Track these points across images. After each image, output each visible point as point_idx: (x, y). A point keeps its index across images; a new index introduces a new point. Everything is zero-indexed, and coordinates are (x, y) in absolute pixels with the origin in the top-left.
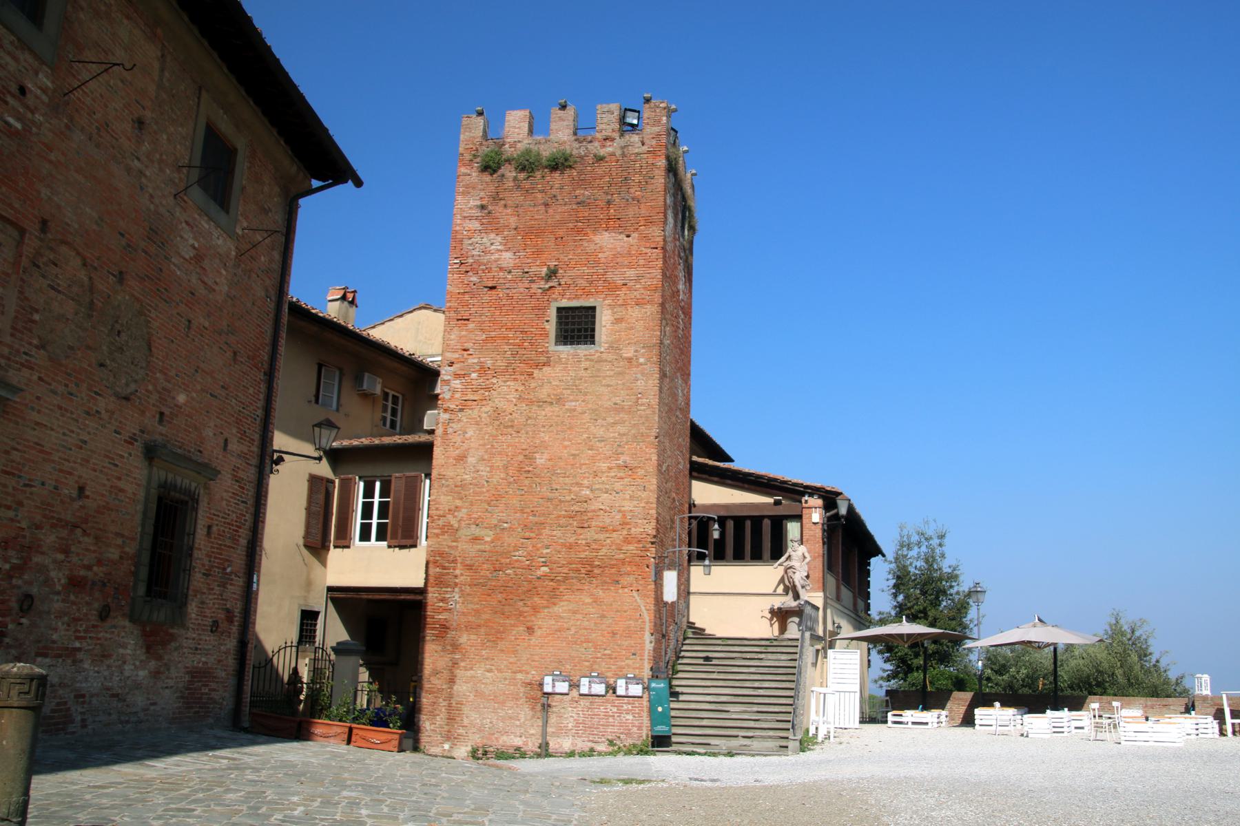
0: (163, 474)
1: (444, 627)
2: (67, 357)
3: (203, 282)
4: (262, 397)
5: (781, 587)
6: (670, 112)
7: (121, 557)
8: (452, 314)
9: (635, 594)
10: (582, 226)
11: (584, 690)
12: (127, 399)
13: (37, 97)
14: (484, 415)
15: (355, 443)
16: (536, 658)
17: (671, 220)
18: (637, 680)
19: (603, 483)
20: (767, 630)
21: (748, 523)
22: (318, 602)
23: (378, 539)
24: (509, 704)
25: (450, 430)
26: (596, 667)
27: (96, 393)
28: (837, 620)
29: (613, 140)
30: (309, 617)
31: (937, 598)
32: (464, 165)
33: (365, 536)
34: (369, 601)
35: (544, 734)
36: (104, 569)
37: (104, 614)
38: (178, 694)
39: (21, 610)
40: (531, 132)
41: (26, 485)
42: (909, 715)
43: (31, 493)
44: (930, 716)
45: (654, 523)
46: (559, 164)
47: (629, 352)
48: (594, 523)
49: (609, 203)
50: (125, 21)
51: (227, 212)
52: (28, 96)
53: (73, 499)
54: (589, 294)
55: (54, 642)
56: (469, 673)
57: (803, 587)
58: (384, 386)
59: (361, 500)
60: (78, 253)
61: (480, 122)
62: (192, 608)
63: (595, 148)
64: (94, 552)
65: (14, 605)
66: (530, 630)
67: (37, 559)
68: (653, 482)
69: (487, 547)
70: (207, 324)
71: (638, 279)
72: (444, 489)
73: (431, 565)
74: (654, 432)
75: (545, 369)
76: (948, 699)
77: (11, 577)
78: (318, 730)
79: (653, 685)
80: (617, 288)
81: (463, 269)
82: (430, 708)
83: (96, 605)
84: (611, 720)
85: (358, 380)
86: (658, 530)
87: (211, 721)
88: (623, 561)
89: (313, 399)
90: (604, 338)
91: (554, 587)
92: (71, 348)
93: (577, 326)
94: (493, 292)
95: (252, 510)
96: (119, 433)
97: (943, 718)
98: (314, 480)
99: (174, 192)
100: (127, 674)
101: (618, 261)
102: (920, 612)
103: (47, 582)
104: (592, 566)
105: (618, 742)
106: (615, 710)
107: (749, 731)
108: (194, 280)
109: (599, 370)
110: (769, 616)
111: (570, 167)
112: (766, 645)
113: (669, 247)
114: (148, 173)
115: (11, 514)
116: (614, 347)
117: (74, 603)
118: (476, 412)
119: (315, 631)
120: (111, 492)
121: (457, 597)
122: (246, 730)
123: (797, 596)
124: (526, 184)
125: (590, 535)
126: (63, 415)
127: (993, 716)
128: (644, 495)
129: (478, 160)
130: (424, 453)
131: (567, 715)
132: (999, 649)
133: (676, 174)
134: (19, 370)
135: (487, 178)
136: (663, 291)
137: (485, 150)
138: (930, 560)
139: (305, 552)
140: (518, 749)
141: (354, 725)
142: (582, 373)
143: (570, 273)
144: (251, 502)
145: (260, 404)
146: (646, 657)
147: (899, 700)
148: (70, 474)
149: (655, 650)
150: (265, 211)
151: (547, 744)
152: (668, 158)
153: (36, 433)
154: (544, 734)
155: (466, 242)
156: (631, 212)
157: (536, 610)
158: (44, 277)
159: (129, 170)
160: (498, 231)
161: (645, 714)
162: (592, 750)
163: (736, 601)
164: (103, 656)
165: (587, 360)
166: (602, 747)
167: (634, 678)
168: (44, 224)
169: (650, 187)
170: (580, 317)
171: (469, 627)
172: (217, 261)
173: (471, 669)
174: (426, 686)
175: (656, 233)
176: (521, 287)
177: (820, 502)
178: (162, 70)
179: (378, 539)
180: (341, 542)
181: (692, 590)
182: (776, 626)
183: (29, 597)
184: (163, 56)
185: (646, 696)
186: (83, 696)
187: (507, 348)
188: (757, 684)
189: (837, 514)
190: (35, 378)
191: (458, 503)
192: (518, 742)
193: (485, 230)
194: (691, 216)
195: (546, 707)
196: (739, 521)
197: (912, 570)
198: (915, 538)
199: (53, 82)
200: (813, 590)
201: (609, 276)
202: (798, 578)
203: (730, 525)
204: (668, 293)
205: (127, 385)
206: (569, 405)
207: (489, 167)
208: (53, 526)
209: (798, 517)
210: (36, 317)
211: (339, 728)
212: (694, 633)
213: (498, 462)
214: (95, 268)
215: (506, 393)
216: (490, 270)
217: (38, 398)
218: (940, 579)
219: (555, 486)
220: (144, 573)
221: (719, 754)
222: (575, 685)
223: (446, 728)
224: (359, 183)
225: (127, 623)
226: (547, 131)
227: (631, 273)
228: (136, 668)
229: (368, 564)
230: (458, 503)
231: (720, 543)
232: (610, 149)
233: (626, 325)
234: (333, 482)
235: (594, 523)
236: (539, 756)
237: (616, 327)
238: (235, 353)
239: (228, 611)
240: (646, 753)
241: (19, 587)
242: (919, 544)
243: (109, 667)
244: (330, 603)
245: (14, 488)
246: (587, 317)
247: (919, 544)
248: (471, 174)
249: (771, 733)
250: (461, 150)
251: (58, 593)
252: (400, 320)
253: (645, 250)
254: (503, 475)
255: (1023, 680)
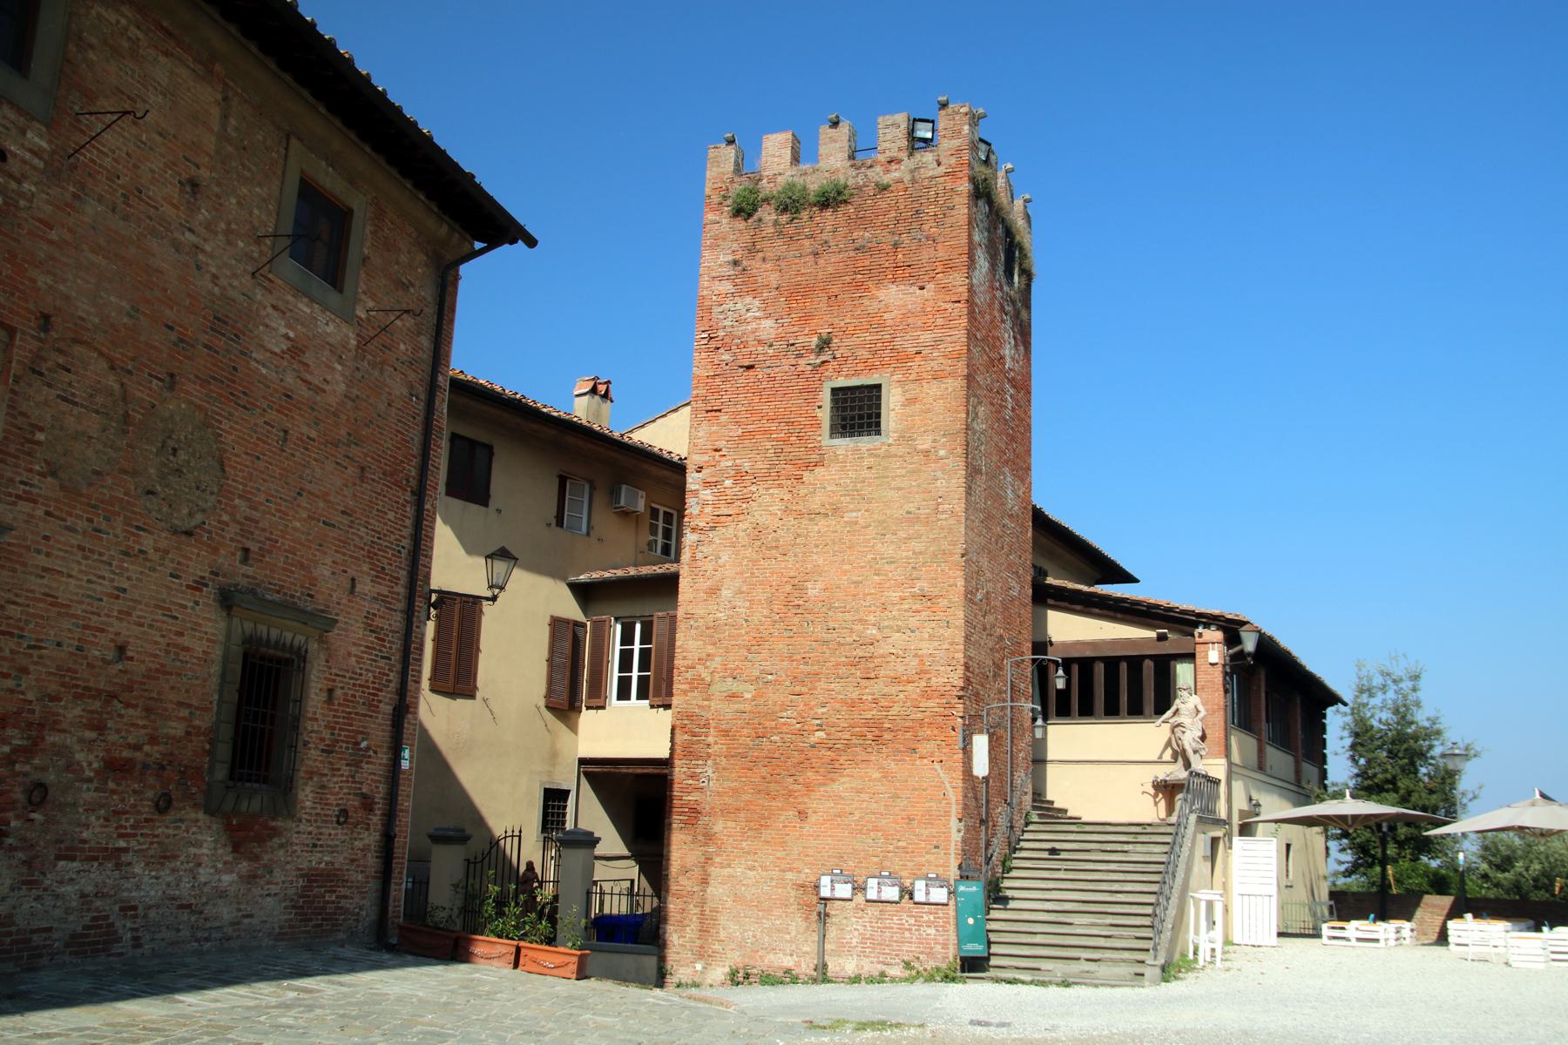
0: (248, 626)
1: (695, 812)
2: (90, 484)
3: (305, 381)
4: (408, 522)
5: (1169, 751)
6: (975, 119)
7: (188, 733)
8: (700, 404)
9: (937, 766)
10: (861, 279)
11: (872, 894)
12: (189, 533)
13: (24, 162)
14: (741, 534)
15: (620, 573)
16: (810, 852)
17: (983, 263)
18: (941, 881)
19: (894, 618)
20: (1149, 810)
21: (1124, 666)
22: (567, 778)
23: (638, 698)
24: (776, 912)
25: (699, 556)
26: (886, 863)
27: (138, 528)
28: (1255, 796)
29: (899, 161)
30: (554, 799)
31: (1412, 763)
32: (712, 210)
33: (624, 694)
34: (637, 776)
35: (822, 952)
36: (161, 748)
37: (164, 805)
38: (288, 903)
39: (30, 802)
40: (796, 159)
41: (30, 647)
42: (1355, 928)
43: (41, 657)
44: (1386, 929)
45: (961, 671)
46: (830, 200)
47: (925, 443)
48: (882, 673)
49: (896, 246)
50: (162, 59)
51: (341, 291)
52: (10, 160)
53: (109, 663)
54: (872, 368)
55: (84, 841)
56: (727, 871)
57: (1195, 752)
58: (649, 499)
59: (618, 647)
60: (101, 354)
61: (730, 152)
62: (306, 795)
63: (877, 174)
64: (144, 727)
65: (19, 795)
66: (802, 815)
67: (52, 738)
68: (959, 616)
69: (748, 707)
70: (314, 434)
71: (935, 345)
72: (693, 632)
73: (677, 731)
74: (959, 549)
75: (817, 470)
76: (1417, 905)
77: (14, 763)
78: (479, 949)
79: (962, 888)
80: (909, 358)
81: (713, 344)
82: (678, 917)
83: (150, 794)
84: (907, 934)
85: (614, 494)
86: (967, 680)
87: (341, 936)
88: (921, 722)
89: (554, 522)
90: (892, 425)
91: (832, 758)
92: (98, 473)
93: (857, 412)
94: (751, 372)
95: (399, 667)
96: (178, 577)
97: (1406, 933)
98: (557, 624)
99: (250, 269)
100: (203, 879)
101: (916, 324)
102: (1387, 781)
103: (71, 766)
104: (880, 729)
105: (916, 965)
106: (912, 921)
107: (1095, 950)
108: (290, 379)
109: (886, 468)
110: (1152, 791)
111: (845, 202)
112: (1139, 831)
113: (980, 300)
114: (208, 248)
115: (10, 683)
116: (906, 438)
117: (113, 792)
118: (731, 530)
119: (564, 815)
120: (167, 652)
121: (710, 773)
122: (391, 949)
123: (1187, 765)
124: (790, 230)
125: (878, 688)
126: (86, 558)
127: (1478, 935)
128: (948, 633)
129: (729, 202)
130: (667, 586)
131: (850, 926)
132: (1503, 835)
133: (990, 202)
134: (14, 504)
135: (740, 224)
136: (970, 359)
137: (737, 188)
138: (1402, 713)
139: (548, 715)
140: (788, 971)
141: (522, 944)
142: (865, 473)
143: (848, 342)
144: (396, 658)
145: (407, 532)
146: (952, 851)
147: (1345, 906)
148: (102, 631)
149: (964, 841)
150: (406, 287)
151: (825, 966)
152: (973, 180)
153: (45, 581)
154: (822, 952)
155: (716, 310)
156: (926, 255)
157: (809, 787)
158: (50, 386)
159: (178, 246)
160: (754, 292)
161: (952, 928)
162: (883, 974)
163: (1102, 770)
164: (165, 857)
165: (871, 455)
166: (896, 971)
167: (937, 878)
168: (46, 321)
169: (949, 221)
170: (861, 400)
171: (727, 812)
172: (327, 353)
173: (729, 866)
174: (673, 887)
175: (958, 281)
176: (786, 364)
177: (1219, 635)
178: (225, 117)
179: (638, 698)
180: (595, 702)
181: (1050, 757)
182: (1162, 804)
183: (41, 786)
184: (225, 99)
185: (952, 903)
186: (135, 908)
187: (768, 445)
188: (1116, 887)
189: (1242, 651)
190: (40, 512)
191: (711, 649)
192: (788, 962)
193: (738, 294)
194: (1024, 256)
195: (823, 917)
196: (1112, 663)
197: (1375, 723)
198: (1378, 681)
199: (50, 142)
200: (1211, 755)
201: (898, 341)
202: (1189, 739)
203: (1075, 668)
204: (981, 360)
205: (191, 515)
206: (848, 517)
207: (744, 210)
208: (77, 696)
209: (1190, 657)
210: (41, 437)
211: (505, 947)
212: (1040, 816)
213: (761, 594)
214: (130, 372)
215: (768, 504)
216: (745, 344)
217: (46, 538)
218: (1416, 738)
219: (831, 625)
220: (224, 751)
221: (1050, 983)
222: (859, 888)
223: (698, 943)
224: (531, 242)
225: (201, 815)
226: (815, 158)
227: (927, 337)
228: (218, 871)
229: (625, 729)
230: (711, 649)
231: (1063, 696)
232: (897, 175)
233: (924, 410)
234: (583, 625)
235: (882, 673)
236: (815, 981)
237: (908, 409)
238: (363, 469)
239: (364, 796)
240: (953, 980)
241: (25, 774)
242: (1384, 688)
243: (173, 870)
244: (583, 780)
245: (12, 652)
246: (870, 399)
247: (1384, 688)
248: (720, 222)
249: (1126, 955)
250: (708, 191)
251: (89, 780)
252: (674, 415)
253: (944, 306)
254: (766, 612)
255: (1535, 880)
